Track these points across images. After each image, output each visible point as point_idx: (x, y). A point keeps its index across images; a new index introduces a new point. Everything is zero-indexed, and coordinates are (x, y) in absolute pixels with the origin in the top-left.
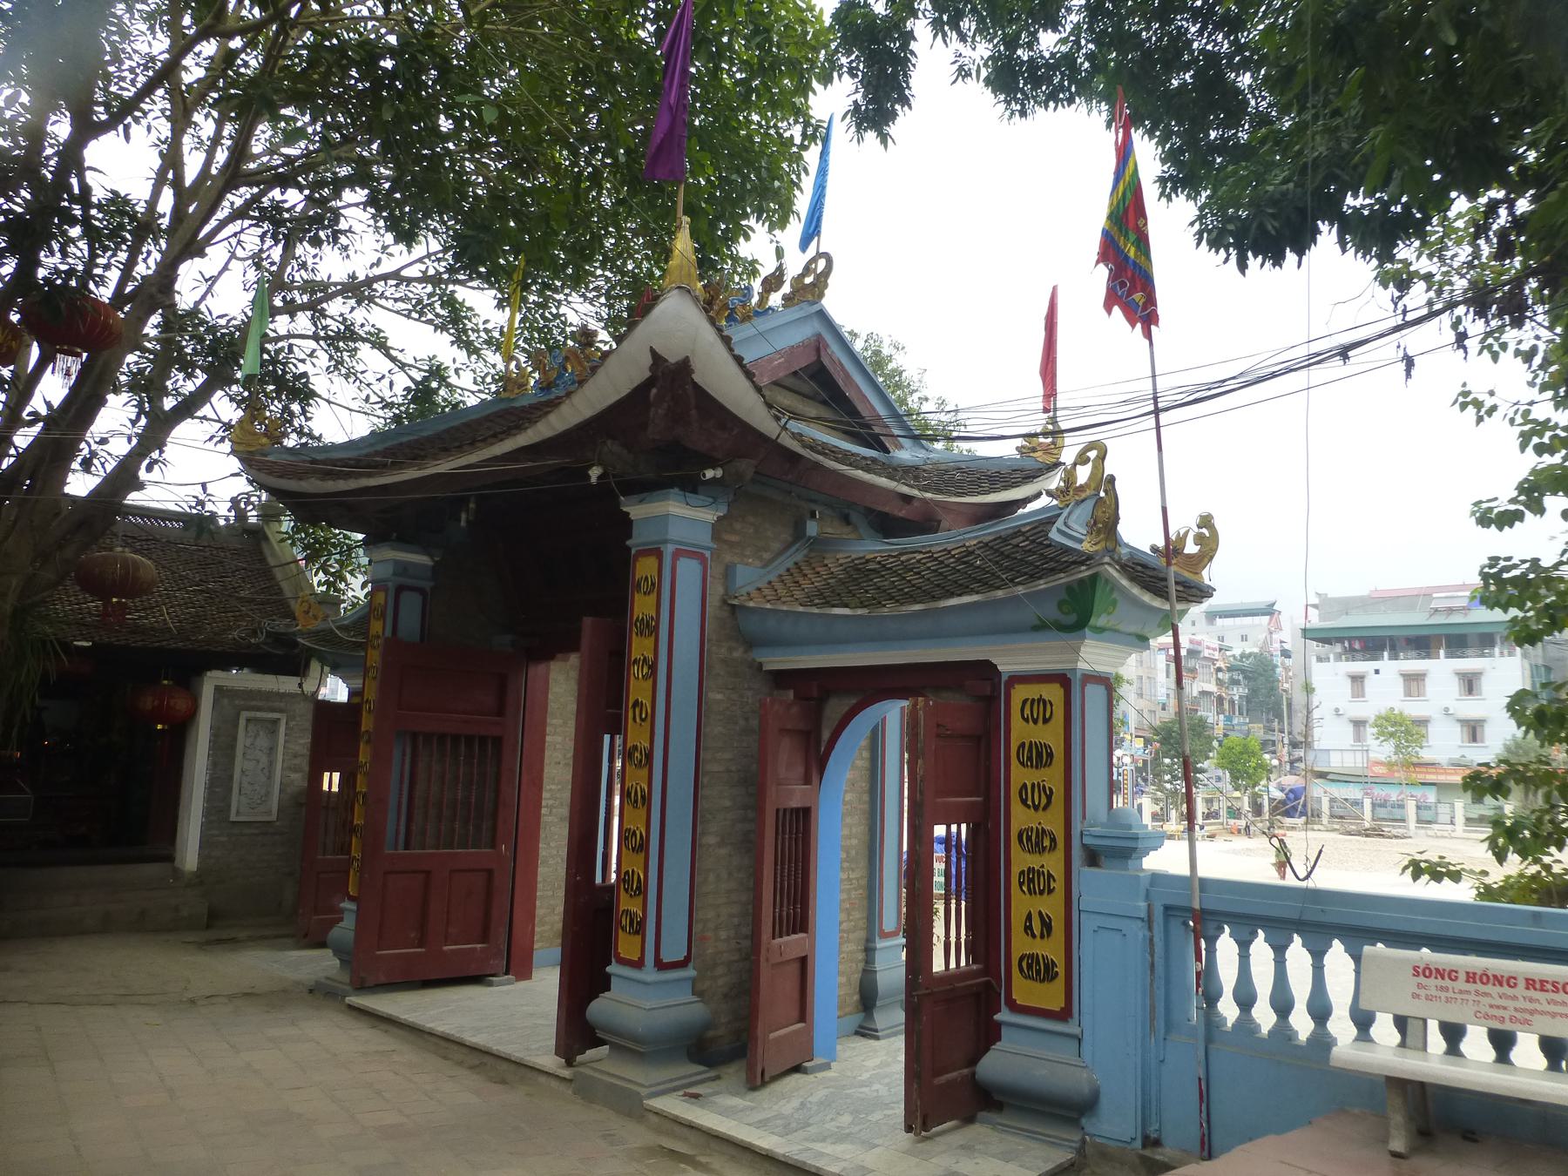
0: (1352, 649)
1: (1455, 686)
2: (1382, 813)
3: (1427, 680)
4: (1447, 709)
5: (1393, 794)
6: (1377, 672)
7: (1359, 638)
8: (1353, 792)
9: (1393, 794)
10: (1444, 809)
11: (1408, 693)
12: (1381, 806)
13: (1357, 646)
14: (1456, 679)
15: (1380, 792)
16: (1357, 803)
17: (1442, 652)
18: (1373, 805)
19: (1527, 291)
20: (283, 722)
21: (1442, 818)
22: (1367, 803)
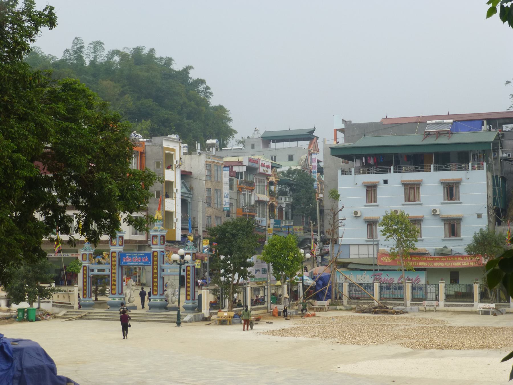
0: (367, 164)
1: (440, 193)
2: (387, 293)
4: (435, 211)
6: (386, 182)
7: (375, 156)
8: (366, 278)
11: (407, 199)
13: (372, 162)
15: (385, 277)
16: (370, 287)
18: (381, 288)
22: (376, 286)
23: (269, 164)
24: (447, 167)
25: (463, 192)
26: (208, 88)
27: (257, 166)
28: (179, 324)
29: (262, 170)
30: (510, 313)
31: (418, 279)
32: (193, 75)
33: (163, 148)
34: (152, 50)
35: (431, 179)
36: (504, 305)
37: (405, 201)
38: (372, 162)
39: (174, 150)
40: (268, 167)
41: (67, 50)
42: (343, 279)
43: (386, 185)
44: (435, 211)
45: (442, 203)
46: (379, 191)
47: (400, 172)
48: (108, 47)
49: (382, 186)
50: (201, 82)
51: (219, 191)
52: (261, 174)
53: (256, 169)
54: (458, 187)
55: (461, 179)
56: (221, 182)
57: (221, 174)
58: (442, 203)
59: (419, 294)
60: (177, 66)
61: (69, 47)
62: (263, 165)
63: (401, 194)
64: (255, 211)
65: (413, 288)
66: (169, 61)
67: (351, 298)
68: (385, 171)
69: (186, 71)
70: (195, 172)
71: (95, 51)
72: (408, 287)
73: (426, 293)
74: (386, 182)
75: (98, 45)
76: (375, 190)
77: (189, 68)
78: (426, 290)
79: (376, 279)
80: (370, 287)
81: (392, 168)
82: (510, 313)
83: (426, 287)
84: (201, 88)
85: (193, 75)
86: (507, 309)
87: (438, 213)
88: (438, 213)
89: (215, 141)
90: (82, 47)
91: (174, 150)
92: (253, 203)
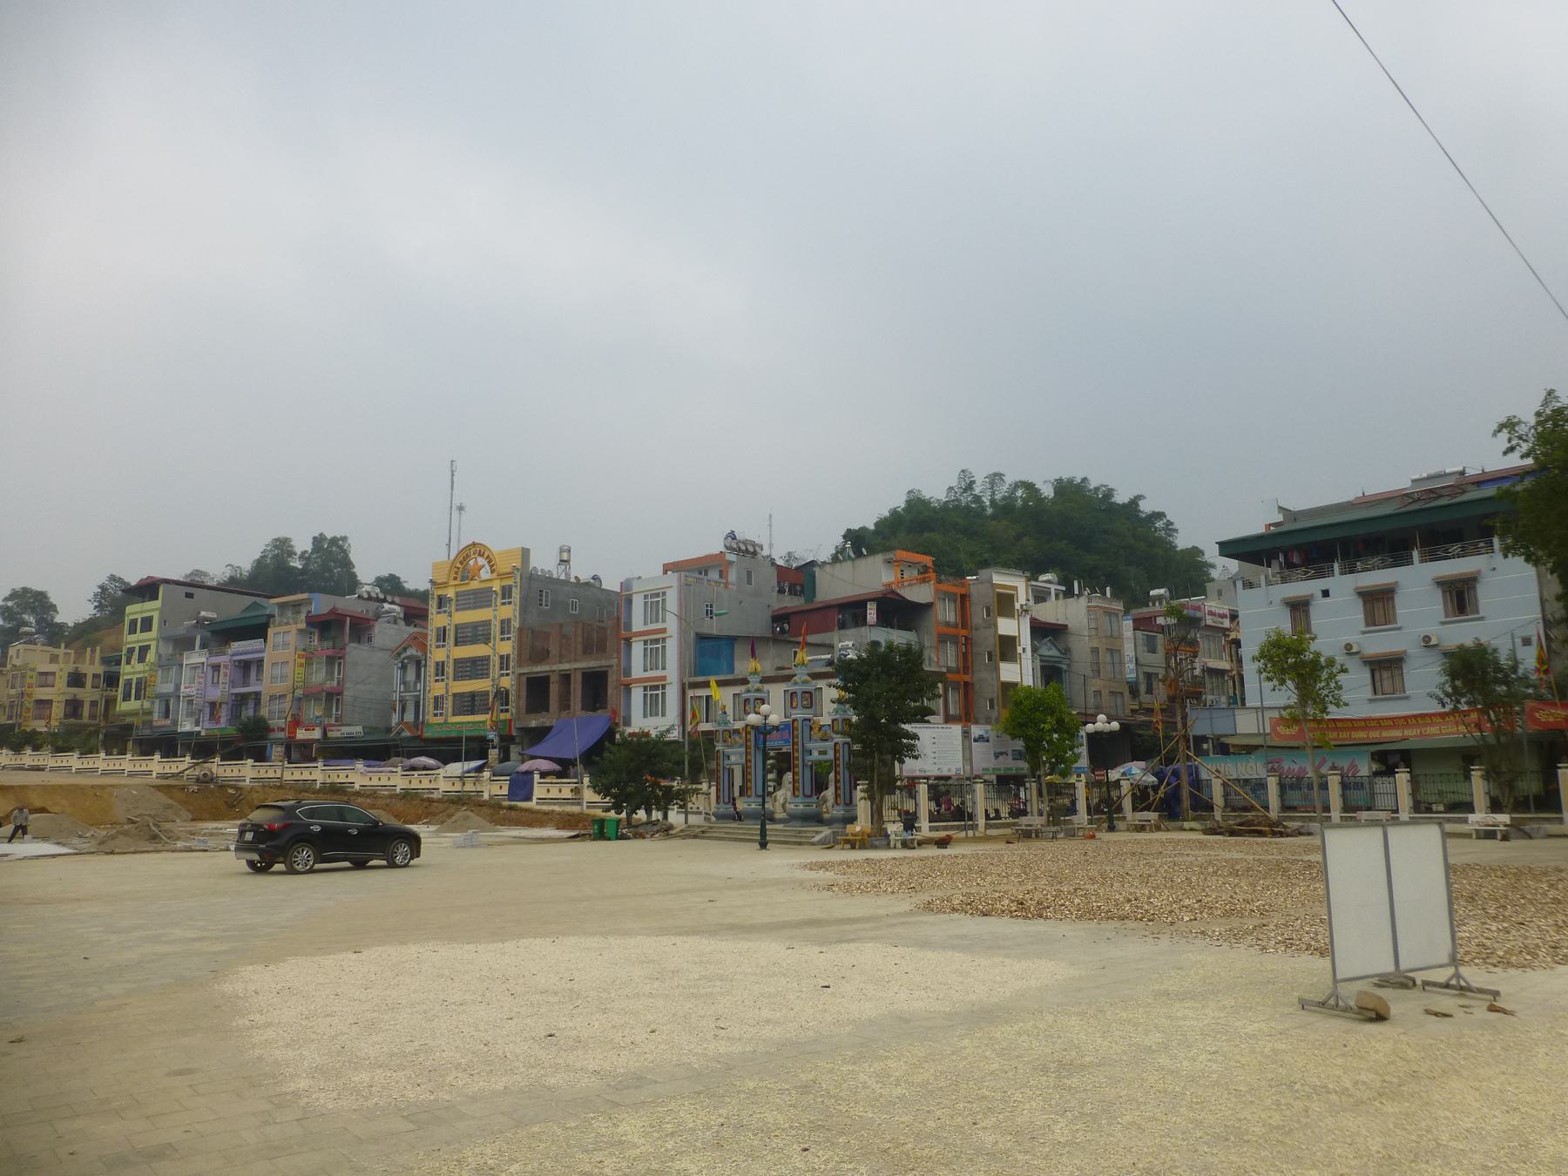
0: (1290, 565)
1: (1436, 604)
2: (1294, 797)
3: (1398, 600)
4: (1427, 639)
5: (1304, 765)
6: (1326, 594)
7: (1298, 548)
8: (1252, 768)
9: (1304, 765)
10: (1382, 785)
11: (1371, 620)
12: (1292, 787)
13: (1296, 559)
14: (1438, 594)
15: (1290, 765)
16: (1259, 786)
17: (1415, 554)
18: (1282, 787)
19: (1083, 733)
20: (730, 718)
21: (1380, 801)
22: (1272, 783)
23: (1226, 612)
24: (1446, 551)
25: (1485, 596)
26: (1170, 523)
27: (1198, 614)
28: (763, 845)
29: (1209, 621)
30: (1565, 836)
31: (1353, 766)
32: (1146, 507)
33: (993, 585)
34: (1084, 480)
35: (1417, 581)
36: (1548, 820)
37: (1367, 625)
38: (1296, 559)
39: (1015, 588)
40: (1223, 616)
41: (951, 488)
42: (1216, 773)
43: (1327, 600)
44: (1427, 639)
45: (1443, 623)
46: (1314, 613)
47: (1352, 572)
48: (1010, 479)
49: (1319, 605)
50: (1160, 515)
51: (1115, 652)
52: (1208, 627)
53: (1199, 620)
54: (1474, 588)
55: (1479, 572)
56: (1120, 637)
57: (1120, 627)
58: (1443, 623)
59: (1357, 796)
60: (1121, 498)
61: (954, 483)
62: (1211, 613)
63: (1357, 613)
64: (1203, 685)
65: (1345, 786)
66: (1109, 493)
67: (1229, 805)
68: (1321, 574)
69: (1134, 502)
70: (1072, 624)
71: (992, 483)
72: (1334, 783)
73: (1373, 795)
74: (1326, 594)
75: (996, 478)
76: (1307, 613)
77: (1139, 497)
78: (1372, 788)
79: (1273, 770)
80: (1259, 786)
81: (1336, 565)
82: (1565, 836)
83: (1371, 784)
84: (1159, 524)
85: (1146, 507)
86: (1553, 828)
87: (1434, 641)
88: (1434, 641)
89: (1162, 591)
90: (973, 482)
91: (1015, 588)
92: (1197, 672)
